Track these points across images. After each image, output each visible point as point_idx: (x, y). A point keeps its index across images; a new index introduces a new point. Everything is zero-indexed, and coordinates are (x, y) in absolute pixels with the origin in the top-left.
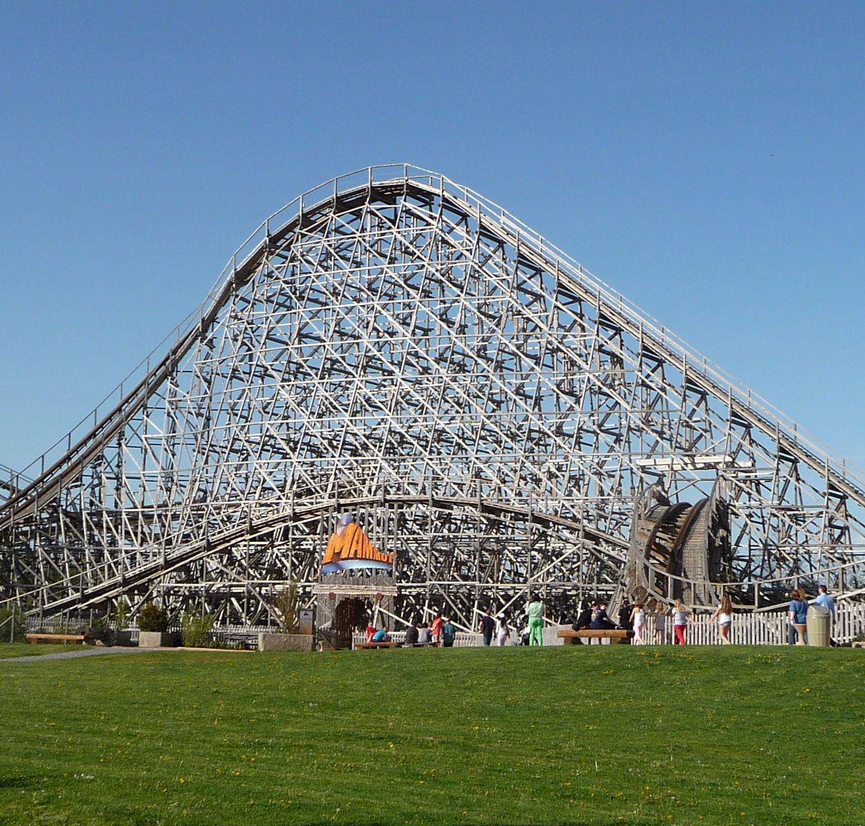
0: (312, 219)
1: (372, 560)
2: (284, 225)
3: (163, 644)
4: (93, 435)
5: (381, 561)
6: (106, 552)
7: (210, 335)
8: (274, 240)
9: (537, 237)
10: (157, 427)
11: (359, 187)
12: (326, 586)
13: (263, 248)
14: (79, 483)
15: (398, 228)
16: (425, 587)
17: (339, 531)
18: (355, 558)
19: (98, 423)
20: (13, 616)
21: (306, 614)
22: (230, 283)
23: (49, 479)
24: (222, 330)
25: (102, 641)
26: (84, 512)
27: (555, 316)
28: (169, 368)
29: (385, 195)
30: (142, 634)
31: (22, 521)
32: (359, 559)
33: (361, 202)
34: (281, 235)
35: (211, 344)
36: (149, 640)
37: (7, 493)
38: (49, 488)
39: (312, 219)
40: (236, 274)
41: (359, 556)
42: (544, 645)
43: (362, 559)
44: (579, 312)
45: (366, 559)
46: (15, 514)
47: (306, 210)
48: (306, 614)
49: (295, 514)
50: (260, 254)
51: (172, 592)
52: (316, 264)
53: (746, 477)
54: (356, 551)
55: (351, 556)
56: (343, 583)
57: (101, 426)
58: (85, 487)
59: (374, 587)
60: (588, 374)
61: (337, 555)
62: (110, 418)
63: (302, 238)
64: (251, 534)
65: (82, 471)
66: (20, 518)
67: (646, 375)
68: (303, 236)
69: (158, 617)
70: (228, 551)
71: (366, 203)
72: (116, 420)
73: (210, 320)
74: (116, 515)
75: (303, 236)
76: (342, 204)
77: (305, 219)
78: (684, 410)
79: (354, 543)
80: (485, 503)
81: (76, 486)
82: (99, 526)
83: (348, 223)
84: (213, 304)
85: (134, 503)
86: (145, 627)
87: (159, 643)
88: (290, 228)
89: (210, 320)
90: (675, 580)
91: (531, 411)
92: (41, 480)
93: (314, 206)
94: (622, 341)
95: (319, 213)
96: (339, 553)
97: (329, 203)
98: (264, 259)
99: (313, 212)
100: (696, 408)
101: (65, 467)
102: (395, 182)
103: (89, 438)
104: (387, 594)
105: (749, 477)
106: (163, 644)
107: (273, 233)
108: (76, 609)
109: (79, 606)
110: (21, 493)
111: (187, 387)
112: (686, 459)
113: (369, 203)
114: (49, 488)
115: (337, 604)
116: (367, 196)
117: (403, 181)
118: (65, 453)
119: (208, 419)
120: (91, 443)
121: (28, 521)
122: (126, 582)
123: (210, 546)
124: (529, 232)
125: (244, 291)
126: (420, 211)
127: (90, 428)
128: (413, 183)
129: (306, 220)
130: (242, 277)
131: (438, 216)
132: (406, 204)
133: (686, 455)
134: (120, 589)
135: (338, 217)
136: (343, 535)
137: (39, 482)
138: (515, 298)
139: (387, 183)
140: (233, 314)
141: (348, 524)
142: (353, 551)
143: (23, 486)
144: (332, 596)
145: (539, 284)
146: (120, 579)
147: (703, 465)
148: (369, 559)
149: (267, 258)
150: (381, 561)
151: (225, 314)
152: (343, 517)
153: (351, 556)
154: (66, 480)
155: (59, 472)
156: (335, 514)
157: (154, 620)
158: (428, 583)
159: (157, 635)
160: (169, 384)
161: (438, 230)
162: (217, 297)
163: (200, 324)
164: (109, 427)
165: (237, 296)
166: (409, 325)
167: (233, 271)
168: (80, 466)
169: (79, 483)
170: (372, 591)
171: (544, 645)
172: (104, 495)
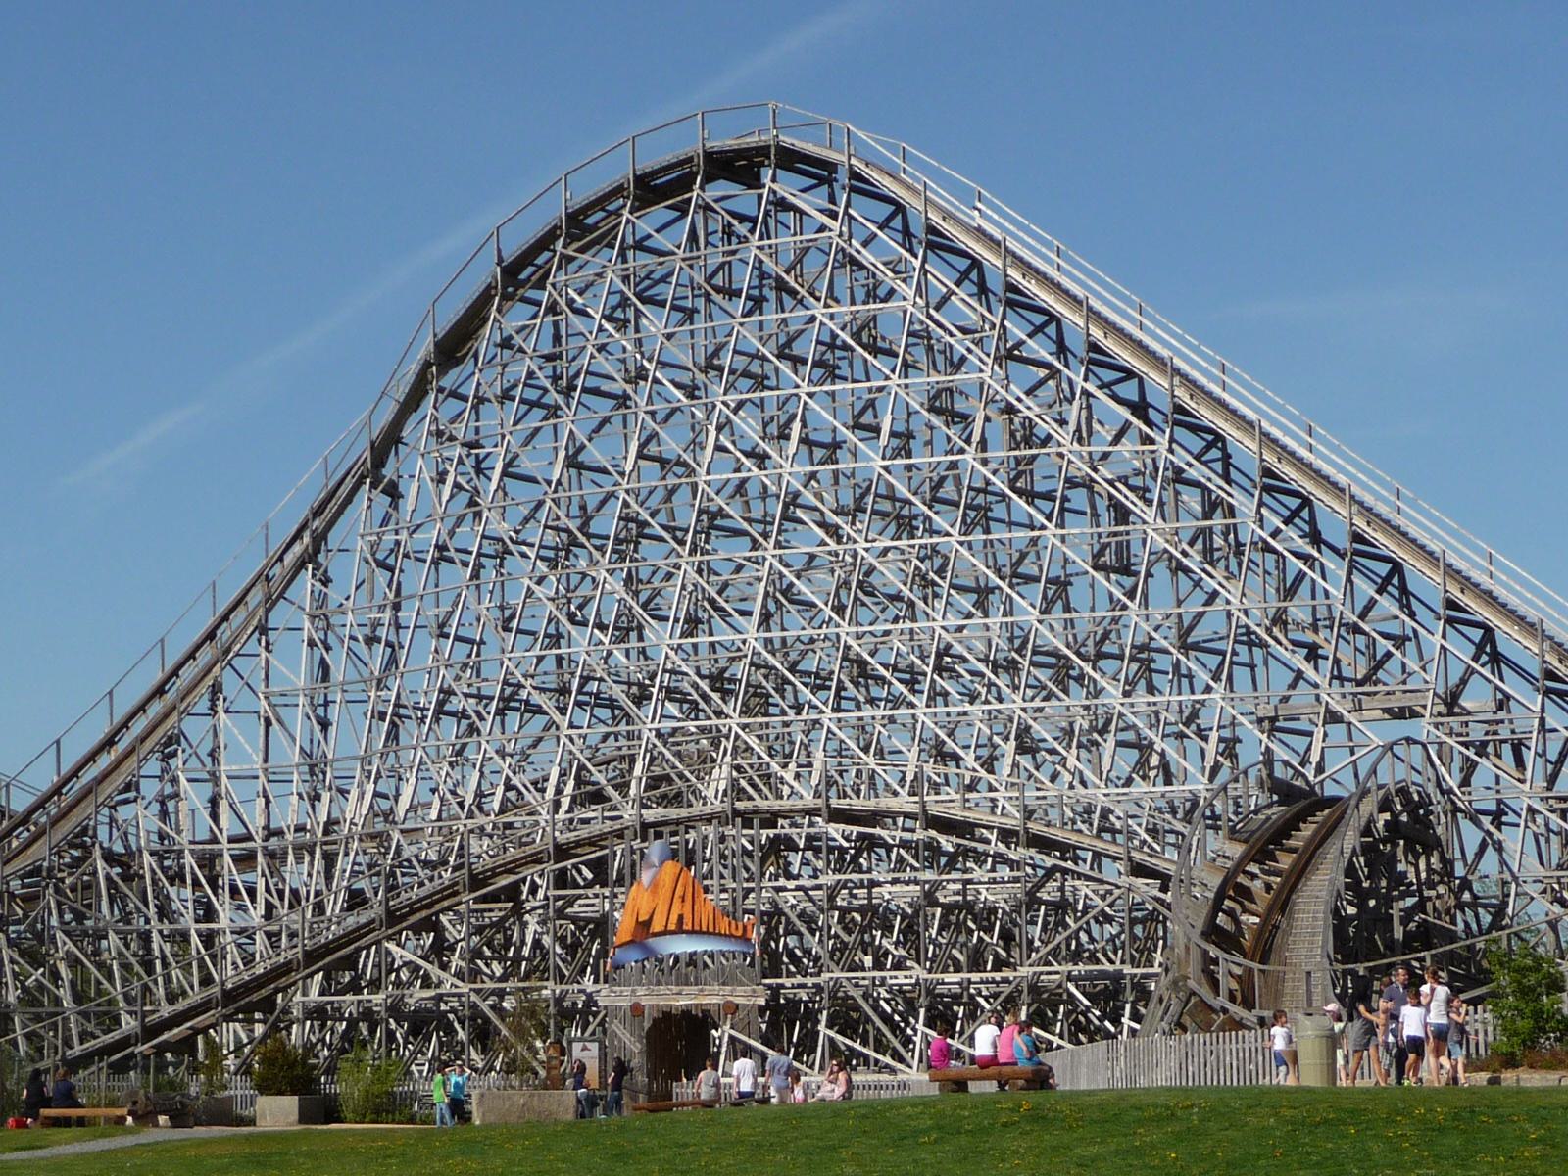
1: (714, 934)
3: (301, 1121)
4: (159, 691)
5: (731, 936)
6: (193, 932)
7: (388, 472)
8: (511, 272)
12: (627, 990)
14: (132, 795)
17: (646, 877)
18: (680, 930)
21: (584, 1048)
22: (427, 365)
32: (687, 932)
33: (685, 184)
34: (527, 257)
38: (71, 808)
41: (687, 927)
42: (1343, 1082)
45: (700, 932)
48: (584, 1048)
50: (484, 299)
54: (681, 918)
55: (672, 927)
61: (644, 927)
62: (192, 655)
76: (649, 189)
79: (677, 901)
87: (295, 1116)
88: (545, 242)
92: (57, 791)
96: (648, 923)
106: (301, 1121)
114: (71, 808)
117: (766, 138)
120: (155, 708)
125: (468, 377)
128: (787, 140)
129: (577, 226)
130: (453, 348)
132: (775, 187)
136: (654, 885)
139: (730, 143)
141: (662, 863)
142: (674, 918)
144: (637, 1010)
148: (707, 933)
150: (731, 936)
152: (655, 849)
159: (290, 1104)
163: (368, 452)
167: (431, 338)
170: (708, 996)
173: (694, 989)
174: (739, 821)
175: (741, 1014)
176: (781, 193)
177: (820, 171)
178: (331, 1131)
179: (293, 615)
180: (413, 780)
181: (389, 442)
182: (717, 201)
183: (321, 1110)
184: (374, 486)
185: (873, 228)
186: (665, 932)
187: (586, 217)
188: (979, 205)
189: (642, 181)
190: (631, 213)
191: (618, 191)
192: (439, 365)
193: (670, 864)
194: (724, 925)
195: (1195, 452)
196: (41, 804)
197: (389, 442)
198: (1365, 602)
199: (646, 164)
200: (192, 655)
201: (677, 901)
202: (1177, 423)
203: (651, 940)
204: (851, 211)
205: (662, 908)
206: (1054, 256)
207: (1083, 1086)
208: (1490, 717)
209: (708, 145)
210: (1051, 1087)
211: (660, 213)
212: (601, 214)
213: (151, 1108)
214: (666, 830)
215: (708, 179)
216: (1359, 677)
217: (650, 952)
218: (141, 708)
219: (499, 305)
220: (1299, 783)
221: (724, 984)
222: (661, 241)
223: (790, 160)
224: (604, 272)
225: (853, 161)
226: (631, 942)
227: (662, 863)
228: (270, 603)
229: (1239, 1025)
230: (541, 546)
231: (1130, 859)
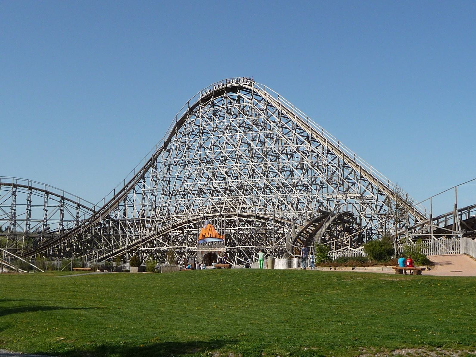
2: (195, 103)
3: (138, 272)
4: (124, 189)
5: (220, 238)
6: (120, 236)
8: (191, 109)
9: (291, 106)
15: (240, 103)
16: (236, 248)
18: (210, 237)
20: (71, 262)
21: (192, 259)
22: (175, 127)
23: (106, 208)
24: (172, 146)
25: (108, 270)
27: (295, 139)
28: (153, 162)
30: (132, 268)
31: (96, 224)
34: (195, 106)
35: (169, 151)
36: (134, 270)
37: (92, 213)
38: (106, 211)
40: (177, 123)
41: (212, 237)
42: (263, 268)
43: (213, 238)
45: (214, 238)
46: (92, 222)
48: (192, 259)
50: (186, 115)
51: (147, 251)
52: (206, 118)
53: (369, 202)
54: (211, 235)
55: (209, 237)
56: (206, 247)
57: (127, 186)
58: (120, 210)
59: (217, 248)
60: (306, 162)
62: (130, 182)
66: (95, 223)
68: (202, 108)
69: (137, 261)
70: (166, 235)
71: (225, 94)
73: (169, 141)
74: (124, 222)
75: (202, 108)
78: (343, 175)
79: (210, 232)
81: (117, 210)
82: (125, 226)
83: (218, 102)
86: (132, 265)
87: (137, 271)
88: (197, 104)
89: (169, 141)
92: (104, 208)
96: (205, 236)
98: (187, 117)
101: (113, 202)
103: (122, 190)
104: (222, 251)
105: (371, 202)
106: (138, 272)
107: (191, 106)
108: (111, 258)
109: (112, 257)
110: (96, 213)
111: (160, 170)
112: (344, 195)
113: (226, 94)
114: (106, 211)
116: (212, 96)
119: (169, 181)
121: (98, 224)
122: (128, 248)
123: (158, 233)
125: (182, 130)
130: (180, 124)
132: (239, 94)
133: (344, 194)
134: (126, 251)
135: (214, 99)
136: (206, 228)
140: (176, 139)
142: (209, 235)
144: (202, 252)
145: (292, 124)
149: (189, 117)
150: (220, 238)
152: (206, 221)
153: (209, 237)
154: (113, 207)
155: (110, 204)
156: (203, 221)
157: (136, 262)
160: (152, 168)
161: (251, 104)
163: (163, 144)
164: (130, 186)
165: (178, 132)
167: (176, 122)
170: (216, 250)
171: (263, 268)
173: (213, 248)
174: (222, 216)
175: (221, 253)
176: (240, 95)
179: (149, 175)
182: (228, 96)
183: (142, 269)
185: (271, 113)
186: (208, 238)
188: (278, 98)
190: (213, 98)
192: (177, 127)
193: (209, 224)
194: (218, 236)
196: (100, 210)
201: (210, 232)
202: (282, 116)
204: (281, 121)
211: (219, 98)
213: (102, 268)
214: (208, 218)
215: (227, 92)
217: (204, 241)
219: (189, 116)
221: (218, 248)
222: (218, 104)
224: (208, 110)
229: (292, 257)
231: (275, 219)
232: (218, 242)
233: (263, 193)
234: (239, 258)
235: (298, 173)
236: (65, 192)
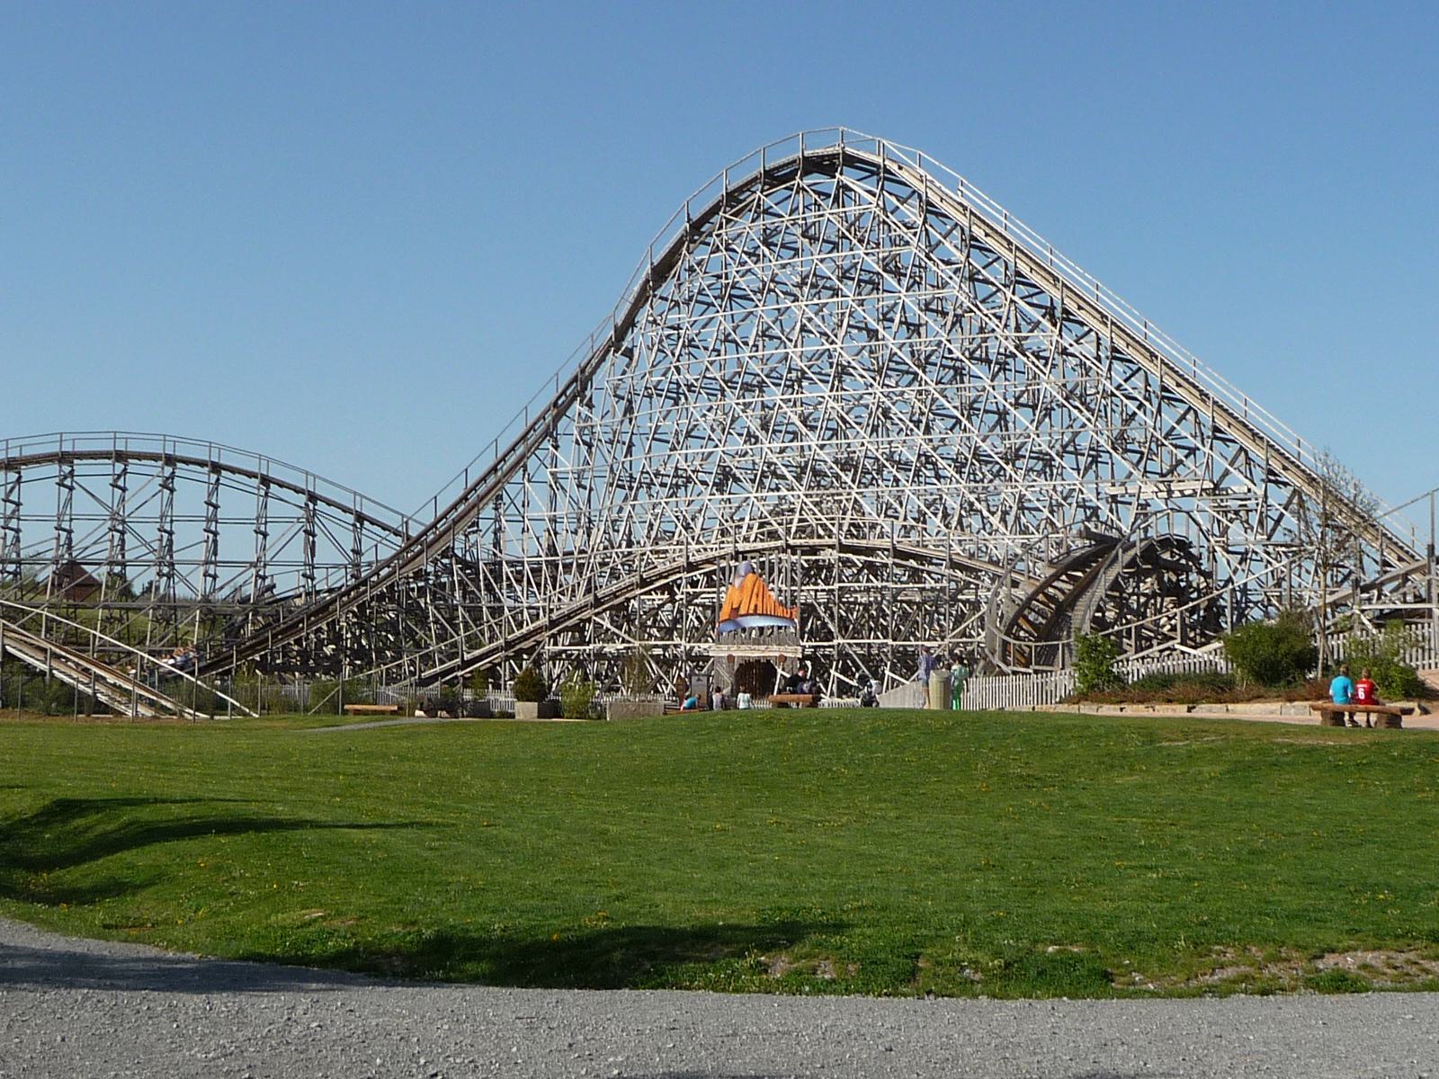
0: (742, 197)
2: (706, 207)
3: (539, 717)
4: (494, 469)
5: (784, 617)
6: (484, 609)
7: (626, 344)
8: (696, 226)
10: (568, 459)
11: (791, 158)
12: (725, 647)
13: (683, 236)
14: (475, 528)
16: (833, 647)
18: (755, 613)
19: (500, 456)
21: (699, 680)
22: (647, 281)
23: (441, 527)
26: (481, 563)
28: (580, 385)
29: (823, 165)
30: (519, 705)
31: (411, 575)
33: (791, 177)
34: (706, 218)
35: (629, 353)
36: (526, 710)
37: (398, 540)
38: (441, 536)
39: (742, 197)
40: (652, 269)
41: (759, 612)
44: (1049, 305)
45: (767, 615)
47: (731, 188)
48: (699, 680)
49: (689, 564)
50: (680, 243)
51: (564, 656)
53: (1241, 506)
54: (756, 606)
55: (751, 612)
56: (743, 644)
57: (503, 459)
59: (775, 647)
60: (1045, 385)
62: (513, 449)
63: (727, 223)
64: (641, 588)
65: (479, 514)
67: (1116, 385)
68: (728, 221)
70: (623, 607)
71: (797, 178)
72: (520, 450)
74: (495, 568)
75: (728, 221)
76: (773, 178)
77: (730, 198)
78: (1158, 425)
80: (899, 547)
81: (474, 532)
82: (498, 579)
84: (627, 306)
85: (1078, 465)
86: (521, 696)
87: (536, 715)
88: (714, 210)
90: (1004, 640)
91: (976, 432)
92: (434, 525)
93: (740, 182)
94: (1099, 339)
95: (749, 190)
96: (738, 609)
97: (756, 178)
98: (684, 252)
99: (741, 189)
100: (1175, 425)
102: (830, 151)
103: (489, 473)
105: (1245, 506)
106: (539, 717)
107: (695, 217)
109: (460, 673)
111: (604, 411)
112: (1161, 486)
114: (441, 536)
115: (736, 668)
117: (837, 150)
118: (461, 493)
119: (631, 445)
121: (419, 575)
122: (509, 645)
124: (990, 206)
125: (668, 288)
126: (859, 186)
127: (489, 461)
128: (849, 150)
129: (732, 197)
130: (661, 272)
131: (878, 192)
132: (842, 178)
135: (766, 196)
136: (742, 587)
137: (431, 528)
138: (967, 291)
139: (820, 151)
140: (651, 319)
141: (746, 574)
142: (752, 607)
143: (414, 533)
144: (731, 658)
146: (502, 641)
147: (1191, 492)
149: (688, 250)
150: (784, 617)
151: (642, 317)
152: (742, 565)
153: (751, 612)
154: (461, 524)
155: (454, 515)
158: (835, 642)
159: (533, 706)
160: (578, 406)
161: (877, 210)
162: (631, 299)
163: (612, 332)
164: (512, 459)
166: (892, 320)
167: (649, 266)
168: (476, 509)
169: (475, 528)
172: (505, 541)
173: (763, 647)
174: (789, 551)
175: (788, 662)
176: (845, 182)
177: (871, 170)
178: (552, 723)
179: (569, 426)
180: (701, 519)
181: (630, 322)
184: (615, 351)
186: (747, 615)
187: (740, 195)
189: (768, 174)
191: (755, 180)
194: (780, 611)
195: (628, 359)
197: (630, 322)
198: (1168, 429)
199: (769, 166)
200: (513, 449)
203: (739, 619)
205: (746, 601)
206: (1003, 219)
207: (906, 706)
208: (1242, 496)
209: (807, 153)
210: (1401, 727)
211: (780, 191)
212: (748, 193)
214: (749, 555)
215: (806, 173)
216: (1164, 471)
217: (738, 624)
218: (484, 479)
219: (688, 246)
220: (1115, 534)
222: (776, 209)
223: (851, 161)
224: (748, 228)
225: (886, 163)
226: (729, 619)
227: (746, 574)
228: (556, 419)
229: (1003, 674)
230: (668, 391)
232: (780, 628)
233: (916, 479)
234: (842, 677)
235: (1022, 419)
236: (320, 478)
